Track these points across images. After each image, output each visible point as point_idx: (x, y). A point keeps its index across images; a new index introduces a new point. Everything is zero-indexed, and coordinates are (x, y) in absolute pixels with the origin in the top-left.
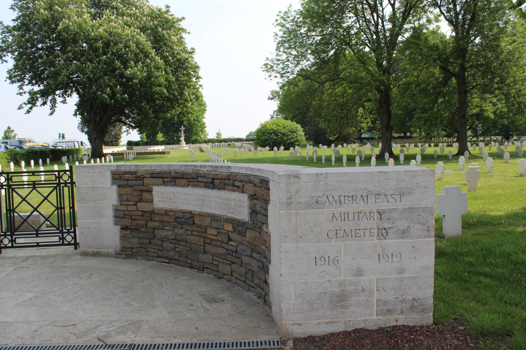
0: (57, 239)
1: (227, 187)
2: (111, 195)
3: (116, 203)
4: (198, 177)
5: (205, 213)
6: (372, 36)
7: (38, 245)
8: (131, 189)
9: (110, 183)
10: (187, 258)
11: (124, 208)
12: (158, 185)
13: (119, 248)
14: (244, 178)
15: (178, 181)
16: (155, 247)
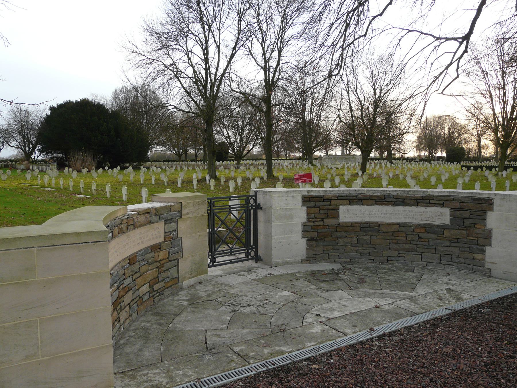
0: (244, 255)
1: (419, 204)
2: (301, 214)
3: (305, 220)
4: (385, 198)
5: (393, 223)
6: (210, 101)
7: (231, 262)
8: (318, 209)
9: (301, 204)
10: (369, 255)
11: (312, 224)
12: (345, 205)
13: (305, 256)
14: (446, 198)
15: (364, 201)
16: (336, 251)
